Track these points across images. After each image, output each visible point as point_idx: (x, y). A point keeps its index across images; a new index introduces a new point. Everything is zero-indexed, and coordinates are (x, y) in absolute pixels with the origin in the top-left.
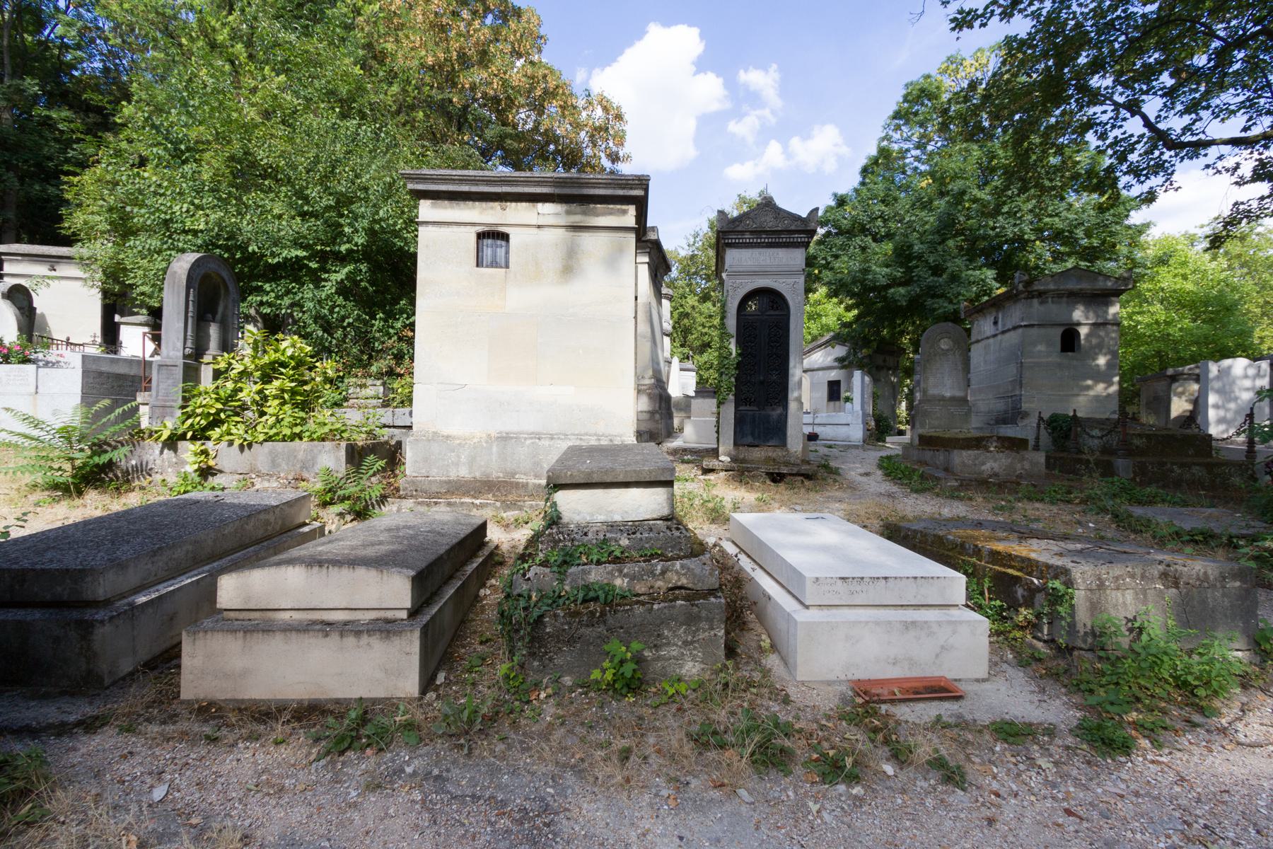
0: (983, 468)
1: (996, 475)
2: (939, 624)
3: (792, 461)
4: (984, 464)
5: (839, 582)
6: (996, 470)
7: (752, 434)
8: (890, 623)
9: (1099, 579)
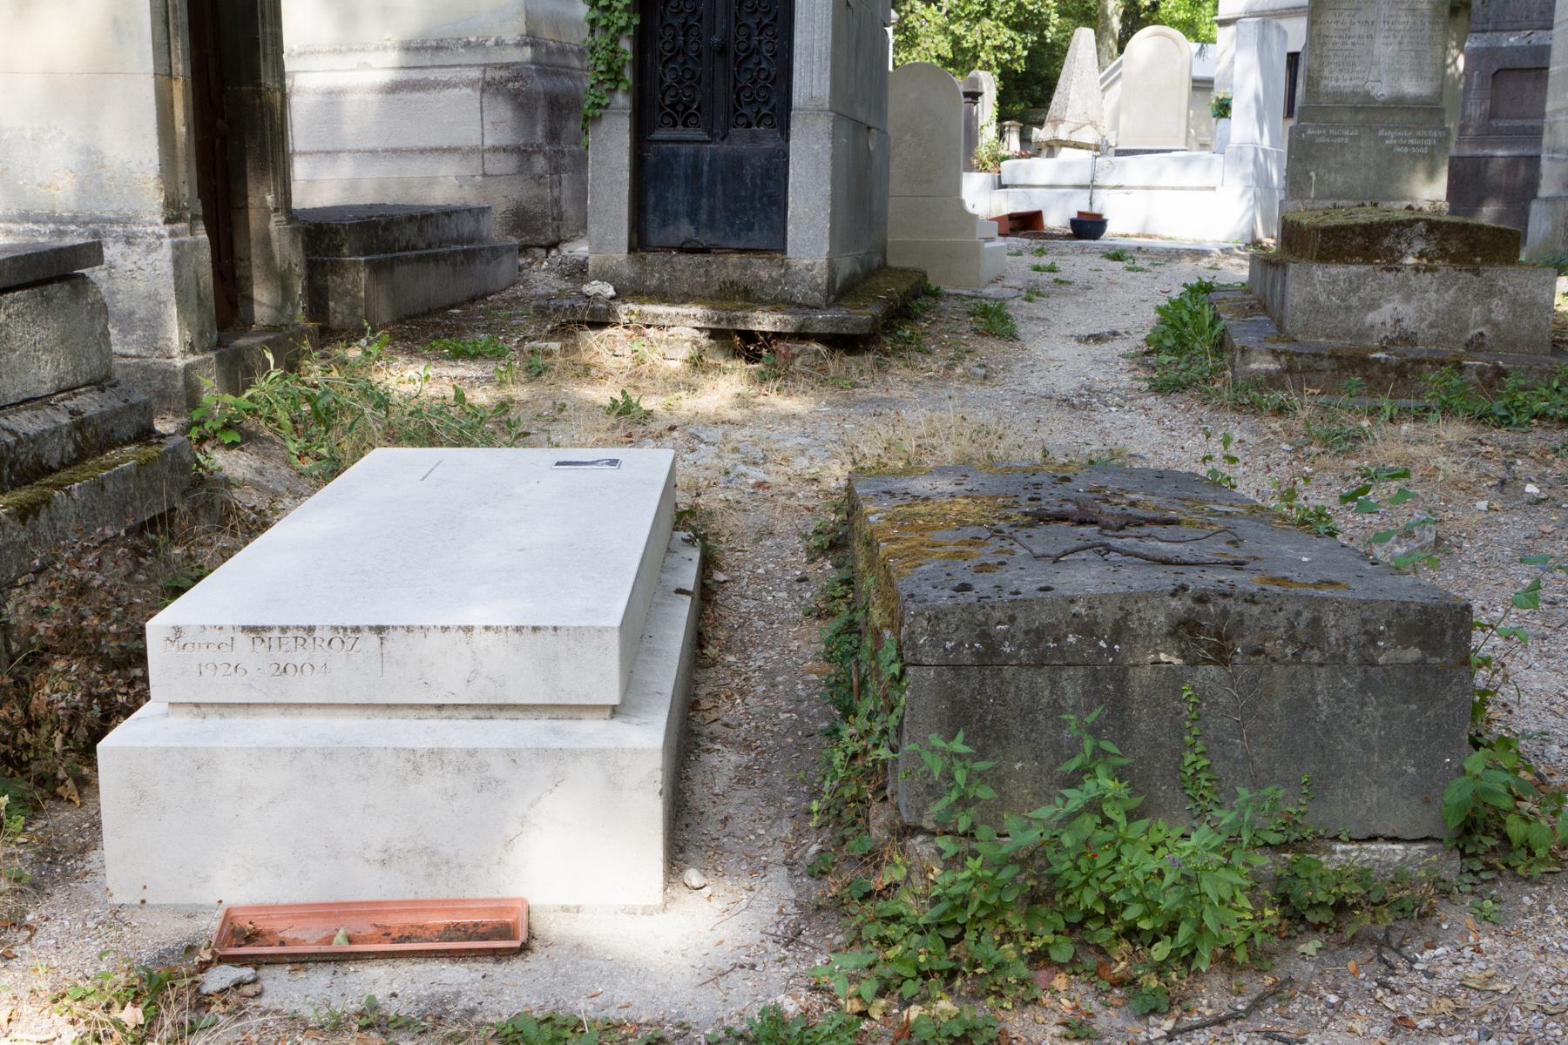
0: (1372, 317)
1: (1408, 339)
2: (512, 757)
3: (799, 293)
4: (1373, 305)
5: (244, 640)
6: (1409, 324)
7: (693, 216)
8: (364, 752)
9: (984, 636)
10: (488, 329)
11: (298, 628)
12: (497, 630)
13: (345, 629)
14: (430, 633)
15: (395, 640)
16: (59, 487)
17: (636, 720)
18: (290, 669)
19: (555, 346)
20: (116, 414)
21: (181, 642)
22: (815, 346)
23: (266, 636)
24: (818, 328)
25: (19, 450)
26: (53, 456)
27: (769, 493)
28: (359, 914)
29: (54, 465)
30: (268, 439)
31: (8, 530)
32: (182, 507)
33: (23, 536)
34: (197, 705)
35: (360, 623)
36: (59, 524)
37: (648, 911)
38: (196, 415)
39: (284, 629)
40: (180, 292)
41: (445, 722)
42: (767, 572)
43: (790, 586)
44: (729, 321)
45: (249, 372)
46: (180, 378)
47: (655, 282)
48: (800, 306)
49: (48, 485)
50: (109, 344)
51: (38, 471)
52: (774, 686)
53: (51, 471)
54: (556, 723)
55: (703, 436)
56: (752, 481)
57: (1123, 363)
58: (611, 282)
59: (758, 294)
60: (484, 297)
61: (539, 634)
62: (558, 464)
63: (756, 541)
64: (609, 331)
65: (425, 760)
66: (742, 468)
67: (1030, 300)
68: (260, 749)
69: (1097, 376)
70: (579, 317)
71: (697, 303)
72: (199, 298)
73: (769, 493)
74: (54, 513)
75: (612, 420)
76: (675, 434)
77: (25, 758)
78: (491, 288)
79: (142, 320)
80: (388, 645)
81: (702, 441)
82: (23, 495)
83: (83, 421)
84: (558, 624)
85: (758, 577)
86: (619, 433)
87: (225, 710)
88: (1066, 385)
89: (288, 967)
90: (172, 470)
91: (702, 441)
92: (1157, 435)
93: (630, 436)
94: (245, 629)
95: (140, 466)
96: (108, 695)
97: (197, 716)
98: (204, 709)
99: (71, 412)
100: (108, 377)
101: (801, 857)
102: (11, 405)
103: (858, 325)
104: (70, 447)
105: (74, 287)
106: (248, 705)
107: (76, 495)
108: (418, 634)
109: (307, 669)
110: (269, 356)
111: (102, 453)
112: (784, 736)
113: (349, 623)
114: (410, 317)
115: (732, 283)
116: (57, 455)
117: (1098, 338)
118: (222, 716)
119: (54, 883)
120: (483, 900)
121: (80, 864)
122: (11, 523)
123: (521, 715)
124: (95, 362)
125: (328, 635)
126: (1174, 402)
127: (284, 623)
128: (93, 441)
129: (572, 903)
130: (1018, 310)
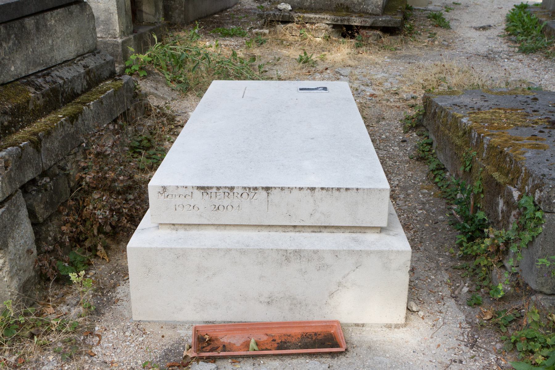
2: (336, 254)
3: (370, 9)
5: (198, 194)
10: (233, 23)
11: (225, 187)
12: (327, 189)
13: (250, 188)
14: (293, 191)
15: (275, 195)
16: (84, 104)
17: (391, 233)
18: (221, 208)
19: (267, 31)
20: (102, 66)
21: (166, 194)
22: (378, 32)
23: (209, 191)
24: (379, 24)
25: (65, 86)
26: (78, 88)
27: (377, 99)
28: (258, 329)
29: (79, 92)
30: (157, 73)
31: (66, 128)
32: (132, 109)
33: (72, 130)
34: (174, 225)
35: (257, 185)
36: (86, 122)
37: (397, 326)
38: (127, 64)
39: (218, 188)
40: (119, 8)
41: (297, 233)
42: (387, 137)
43: (399, 144)
44: (341, 21)
45: (146, 44)
46: (120, 47)
47: (308, 4)
48: (370, 14)
49: (78, 103)
50: (96, 34)
51: (73, 96)
52: (408, 195)
53: (78, 95)
54: (354, 235)
55: (341, 72)
56: (368, 94)
57: (500, 40)
58: (289, 4)
59: (353, 9)
60: (226, 9)
61: (349, 192)
62: (301, 89)
63: (378, 122)
64: (290, 25)
65: (292, 255)
66: (363, 88)
67: (448, 11)
68: (208, 249)
69: (492, 45)
70: (277, 19)
71: (327, 13)
72: (126, 11)
73: (377, 99)
74: (84, 118)
75: (301, 65)
76: (328, 71)
77: (81, 238)
78: (228, 6)
79: (103, 21)
80: (271, 197)
81: (341, 75)
82: (70, 109)
83: (89, 71)
84: (359, 187)
85: (383, 139)
86: (304, 71)
87: (187, 227)
88: (483, 50)
89: (230, 361)
90: (127, 92)
91: (341, 75)
92: (531, 74)
93: (309, 72)
94: (198, 188)
95: (115, 91)
96: (119, 209)
97: (173, 229)
98: (177, 226)
99: (84, 67)
100: (96, 49)
101: (459, 293)
102: (59, 64)
103: (396, 23)
104: (85, 83)
105: (81, 7)
106: (199, 225)
107: (92, 107)
108: (287, 191)
109: (230, 207)
110: (155, 37)
111: (97, 85)
112: (424, 223)
113: (252, 185)
114: (200, 18)
115: (341, 4)
116: (80, 87)
117: (484, 28)
118: (186, 229)
119: (104, 306)
120: (318, 322)
121: (114, 295)
122: (67, 125)
123: (335, 231)
124: (91, 42)
125: (240, 191)
126: (532, 57)
127: (218, 185)
128: (93, 79)
129: (360, 322)
130: (447, 16)
